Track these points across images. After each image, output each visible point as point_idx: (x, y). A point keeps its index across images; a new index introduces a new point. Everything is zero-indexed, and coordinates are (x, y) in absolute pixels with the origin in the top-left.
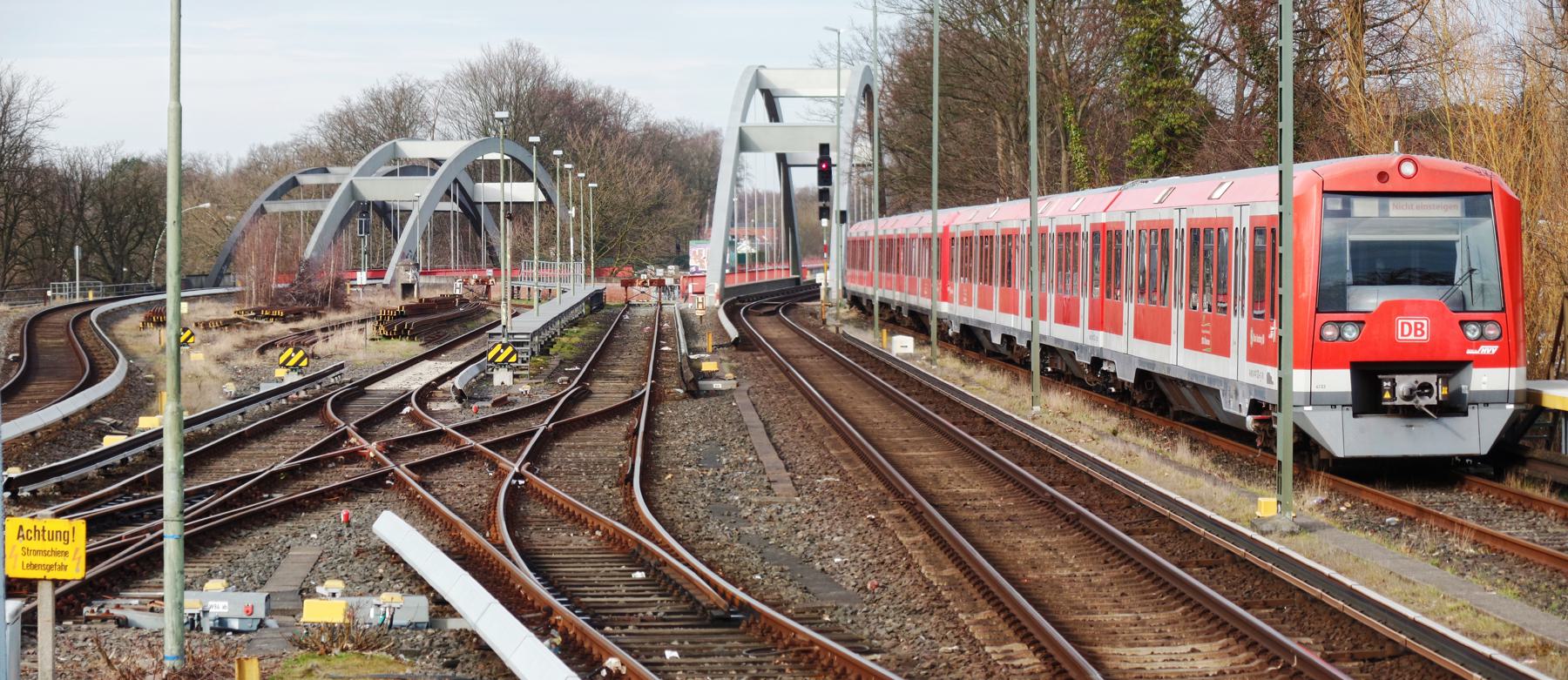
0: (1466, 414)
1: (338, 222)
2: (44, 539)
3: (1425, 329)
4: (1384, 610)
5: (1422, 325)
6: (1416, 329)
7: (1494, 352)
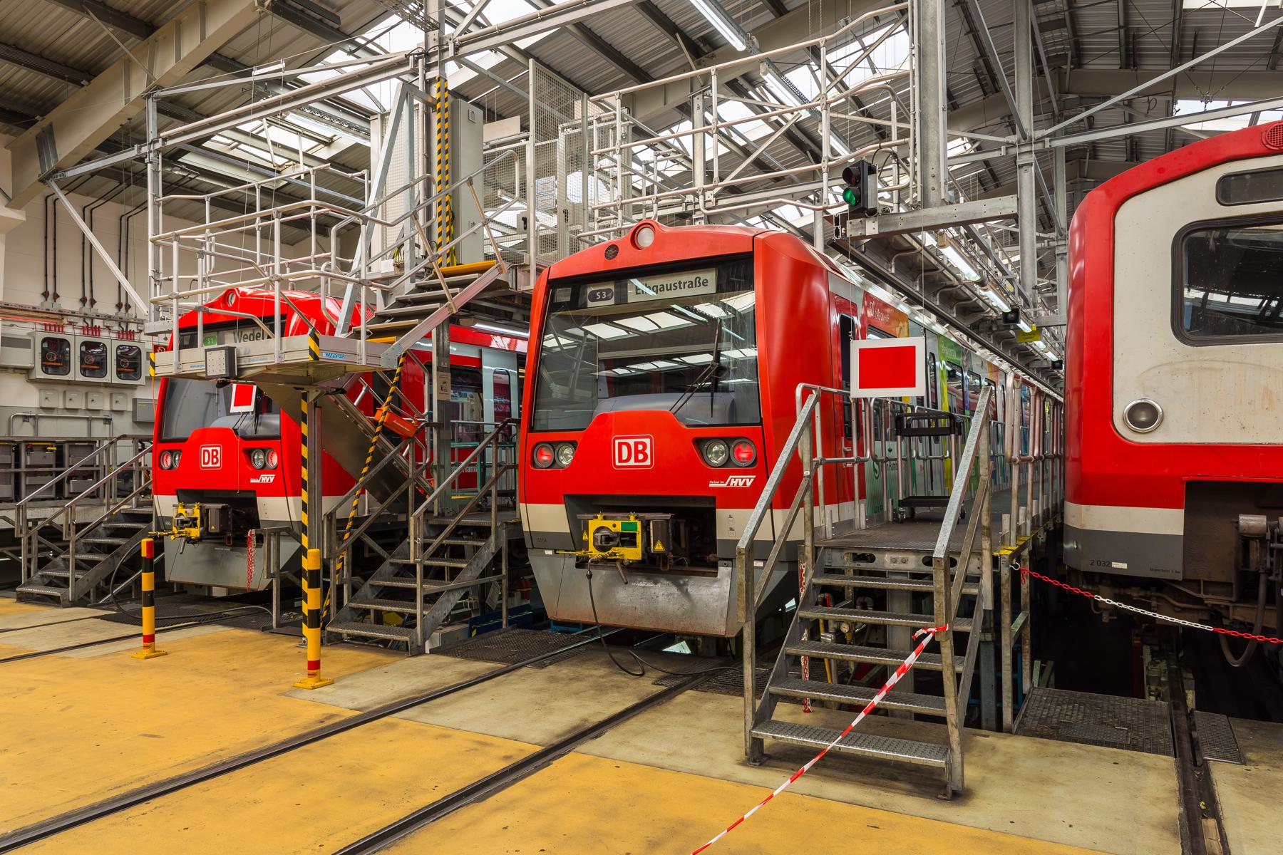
0: (939, 642)
1: (1165, 419)
2: (681, 288)
3: (648, 451)
4: (551, 40)
5: (644, 445)
6: (637, 452)
7: (749, 484)
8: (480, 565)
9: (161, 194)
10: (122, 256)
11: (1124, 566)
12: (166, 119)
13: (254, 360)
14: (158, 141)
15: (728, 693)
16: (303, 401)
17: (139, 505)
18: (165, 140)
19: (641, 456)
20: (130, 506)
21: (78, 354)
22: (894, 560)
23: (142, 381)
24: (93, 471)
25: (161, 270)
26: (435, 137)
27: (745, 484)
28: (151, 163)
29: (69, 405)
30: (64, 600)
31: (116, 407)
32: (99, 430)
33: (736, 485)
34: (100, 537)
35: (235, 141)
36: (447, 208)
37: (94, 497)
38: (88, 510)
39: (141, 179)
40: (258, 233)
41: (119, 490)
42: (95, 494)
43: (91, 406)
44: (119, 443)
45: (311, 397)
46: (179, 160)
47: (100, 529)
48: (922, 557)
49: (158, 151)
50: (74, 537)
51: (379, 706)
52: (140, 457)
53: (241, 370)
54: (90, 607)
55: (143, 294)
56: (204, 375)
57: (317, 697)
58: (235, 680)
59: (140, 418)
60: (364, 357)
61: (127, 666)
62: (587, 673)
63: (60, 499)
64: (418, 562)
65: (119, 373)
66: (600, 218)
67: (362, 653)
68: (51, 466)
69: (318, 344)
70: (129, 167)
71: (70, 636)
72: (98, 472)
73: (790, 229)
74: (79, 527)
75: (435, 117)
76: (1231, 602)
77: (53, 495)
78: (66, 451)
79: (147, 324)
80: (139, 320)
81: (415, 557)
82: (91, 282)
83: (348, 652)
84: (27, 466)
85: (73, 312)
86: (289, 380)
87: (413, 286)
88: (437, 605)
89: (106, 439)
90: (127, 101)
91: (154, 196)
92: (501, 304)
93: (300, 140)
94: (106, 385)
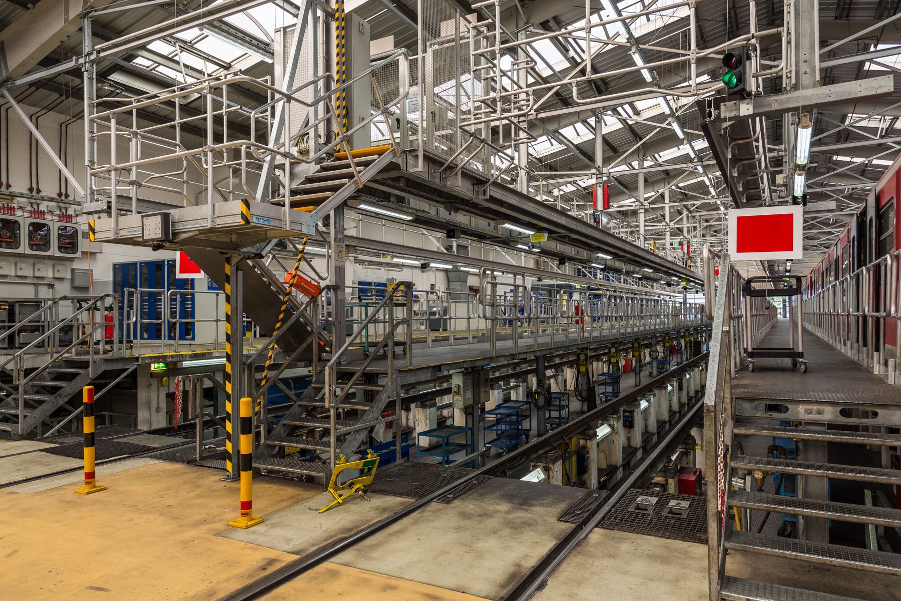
8: (379, 407)
9: (95, 98)
10: (63, 153)
12: (97, 40)
13: (187, 225)
14: (92, 53)
15: (634, 532)
16: (226, 264)
17: (77, 354)
18: (98, 52)
20: (71, 354)
21: (27, 232)
22: (809, 412)
23: (79, 254)
24: (39, 326)
25: (96, 161)
26: (334, 42)
28: (87, 71)
29: (20, 273)
30: (14, 434)
31: (57, 276)
32: (44, 293)
34: (45, 380)
35: (155, 62)
36: (344, 103)
37: (40, 347)
38: (35, 357)
39: (78, 93)
40: (178, 128)
41: (60, 341)
42: (41, 344)
43: (38, 274)
44: (61, 303)
45: (234, 261)
46: (109, 78)
47: (45, 374)
48: (840, 408)
49: (92, 61)
50: (23, 381)
51: (316, 548)
52: (78, 314)
53: (175, 234)
54: (37, 440)
55: (83, 184)
56: (141, 239)
57: (253, 537)
58: (172, 518)
59: (77, 284)
60: (288, 223)
61: (69, 502)
62: (491, 508)
63: (12, 348)
64: (331, 407)
65: (60, 248)
66: (476, 112)
67: (282, 488)
68: (4, 322)
69: (249, 210)
70: (69, 83)
71: (18, 470)
72: (43, 326)
73: (570, 145)
74: (28, 372)
75: (334, 25)
77: (6, 346)
78: (17, 309)
79: (84, 205)
80: (77, 202)
81: (330, 403)
82: (37, 175)
83: (268, 486)
85: (22, 194)
86: (215, 245)
87: (318, 167)
88: (346, 444)
89: (50, 299)
90: (66, 20)
91: (89, 99)
92: (388, 186)
93: (205, 64)
94: (50, 258)
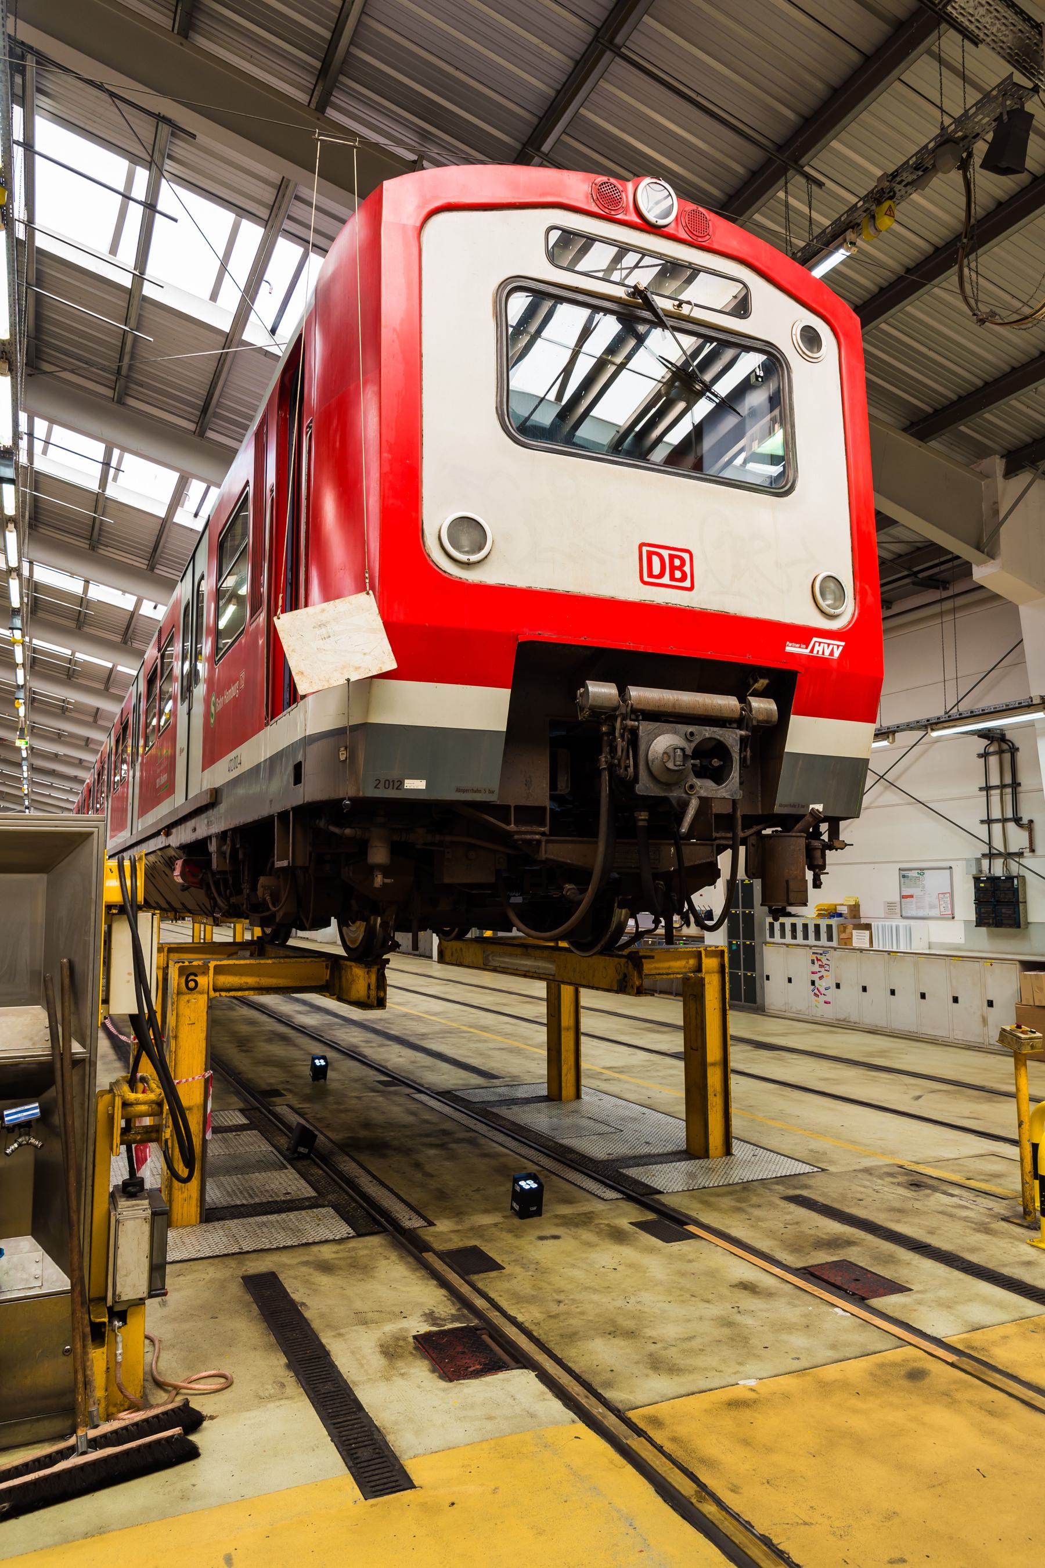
6: (673, 568)
11: (420, 784)
19: (678, 574)
27: (832, 653)
33: (821, 653)
76: (543, 834)
84: (781, 805)
